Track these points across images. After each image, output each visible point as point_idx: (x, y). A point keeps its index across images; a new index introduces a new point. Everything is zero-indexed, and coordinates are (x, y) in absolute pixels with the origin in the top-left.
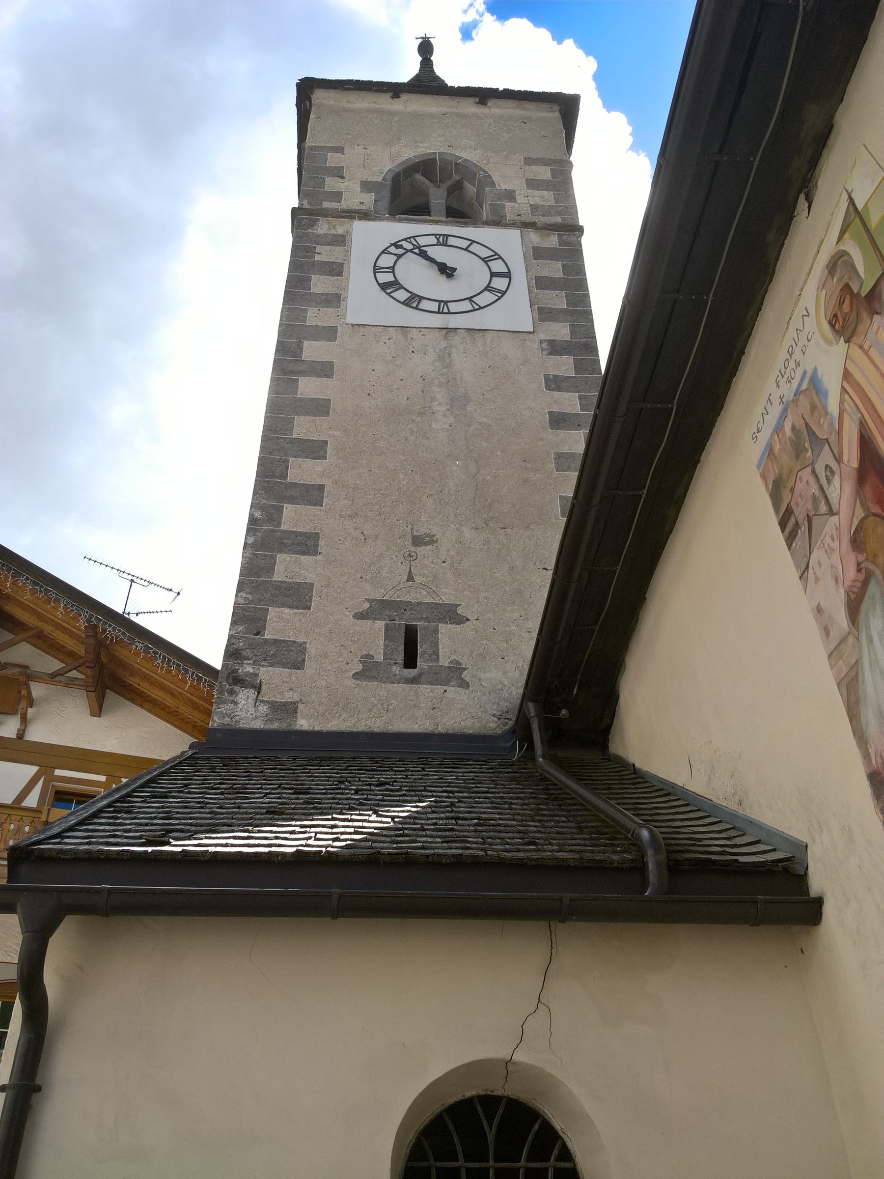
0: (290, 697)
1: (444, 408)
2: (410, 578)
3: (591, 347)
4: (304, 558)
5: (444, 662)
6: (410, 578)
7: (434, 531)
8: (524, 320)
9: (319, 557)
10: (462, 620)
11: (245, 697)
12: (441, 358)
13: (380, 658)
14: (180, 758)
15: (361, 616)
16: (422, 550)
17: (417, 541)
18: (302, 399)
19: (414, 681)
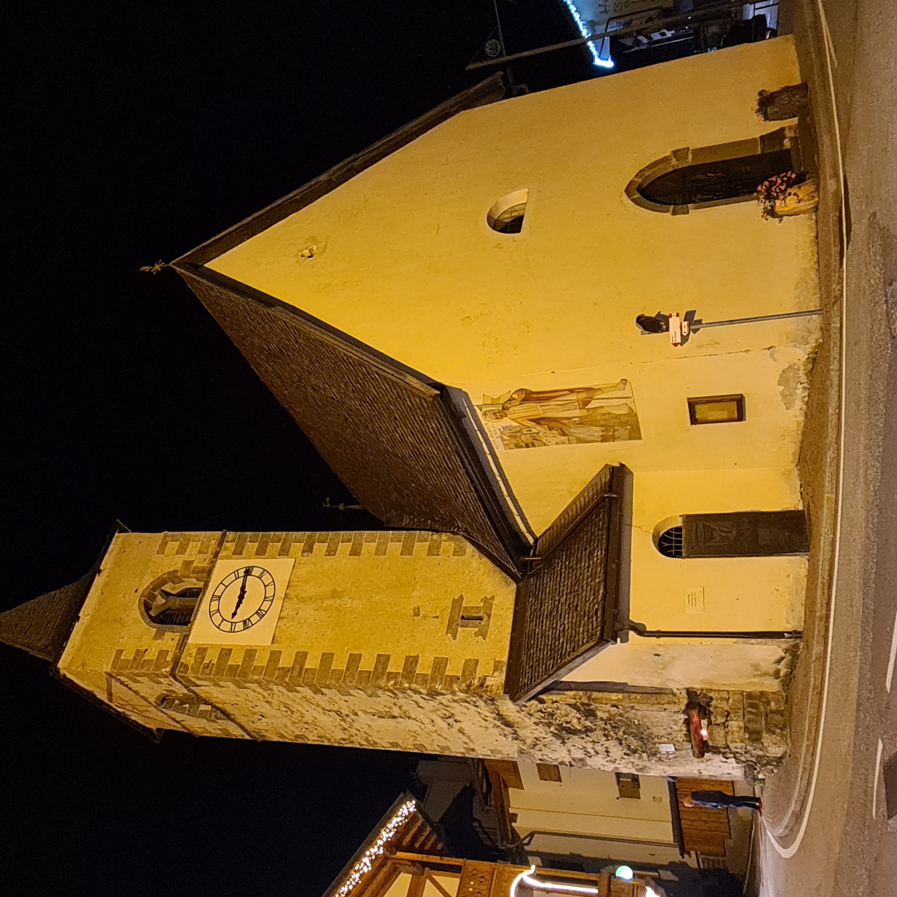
0: (492, 664)
1: (338, 601)
2: (437, 617)
3: (882, 740)
4: (419, 662)
5: (482, 604)
6: (437, 617)
7: (413, 607)
8: (287, 563)
9: (420, 655)
10: (462, 597)
11: (489, 681)
12: (304, 602)
13: (477, 629)
14: (363, 847)
15: (454, 637)
16: (422, 612)
17: (417, 614)
18: (320, 666)
19: (489, 616)
